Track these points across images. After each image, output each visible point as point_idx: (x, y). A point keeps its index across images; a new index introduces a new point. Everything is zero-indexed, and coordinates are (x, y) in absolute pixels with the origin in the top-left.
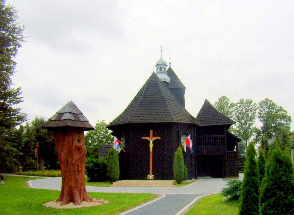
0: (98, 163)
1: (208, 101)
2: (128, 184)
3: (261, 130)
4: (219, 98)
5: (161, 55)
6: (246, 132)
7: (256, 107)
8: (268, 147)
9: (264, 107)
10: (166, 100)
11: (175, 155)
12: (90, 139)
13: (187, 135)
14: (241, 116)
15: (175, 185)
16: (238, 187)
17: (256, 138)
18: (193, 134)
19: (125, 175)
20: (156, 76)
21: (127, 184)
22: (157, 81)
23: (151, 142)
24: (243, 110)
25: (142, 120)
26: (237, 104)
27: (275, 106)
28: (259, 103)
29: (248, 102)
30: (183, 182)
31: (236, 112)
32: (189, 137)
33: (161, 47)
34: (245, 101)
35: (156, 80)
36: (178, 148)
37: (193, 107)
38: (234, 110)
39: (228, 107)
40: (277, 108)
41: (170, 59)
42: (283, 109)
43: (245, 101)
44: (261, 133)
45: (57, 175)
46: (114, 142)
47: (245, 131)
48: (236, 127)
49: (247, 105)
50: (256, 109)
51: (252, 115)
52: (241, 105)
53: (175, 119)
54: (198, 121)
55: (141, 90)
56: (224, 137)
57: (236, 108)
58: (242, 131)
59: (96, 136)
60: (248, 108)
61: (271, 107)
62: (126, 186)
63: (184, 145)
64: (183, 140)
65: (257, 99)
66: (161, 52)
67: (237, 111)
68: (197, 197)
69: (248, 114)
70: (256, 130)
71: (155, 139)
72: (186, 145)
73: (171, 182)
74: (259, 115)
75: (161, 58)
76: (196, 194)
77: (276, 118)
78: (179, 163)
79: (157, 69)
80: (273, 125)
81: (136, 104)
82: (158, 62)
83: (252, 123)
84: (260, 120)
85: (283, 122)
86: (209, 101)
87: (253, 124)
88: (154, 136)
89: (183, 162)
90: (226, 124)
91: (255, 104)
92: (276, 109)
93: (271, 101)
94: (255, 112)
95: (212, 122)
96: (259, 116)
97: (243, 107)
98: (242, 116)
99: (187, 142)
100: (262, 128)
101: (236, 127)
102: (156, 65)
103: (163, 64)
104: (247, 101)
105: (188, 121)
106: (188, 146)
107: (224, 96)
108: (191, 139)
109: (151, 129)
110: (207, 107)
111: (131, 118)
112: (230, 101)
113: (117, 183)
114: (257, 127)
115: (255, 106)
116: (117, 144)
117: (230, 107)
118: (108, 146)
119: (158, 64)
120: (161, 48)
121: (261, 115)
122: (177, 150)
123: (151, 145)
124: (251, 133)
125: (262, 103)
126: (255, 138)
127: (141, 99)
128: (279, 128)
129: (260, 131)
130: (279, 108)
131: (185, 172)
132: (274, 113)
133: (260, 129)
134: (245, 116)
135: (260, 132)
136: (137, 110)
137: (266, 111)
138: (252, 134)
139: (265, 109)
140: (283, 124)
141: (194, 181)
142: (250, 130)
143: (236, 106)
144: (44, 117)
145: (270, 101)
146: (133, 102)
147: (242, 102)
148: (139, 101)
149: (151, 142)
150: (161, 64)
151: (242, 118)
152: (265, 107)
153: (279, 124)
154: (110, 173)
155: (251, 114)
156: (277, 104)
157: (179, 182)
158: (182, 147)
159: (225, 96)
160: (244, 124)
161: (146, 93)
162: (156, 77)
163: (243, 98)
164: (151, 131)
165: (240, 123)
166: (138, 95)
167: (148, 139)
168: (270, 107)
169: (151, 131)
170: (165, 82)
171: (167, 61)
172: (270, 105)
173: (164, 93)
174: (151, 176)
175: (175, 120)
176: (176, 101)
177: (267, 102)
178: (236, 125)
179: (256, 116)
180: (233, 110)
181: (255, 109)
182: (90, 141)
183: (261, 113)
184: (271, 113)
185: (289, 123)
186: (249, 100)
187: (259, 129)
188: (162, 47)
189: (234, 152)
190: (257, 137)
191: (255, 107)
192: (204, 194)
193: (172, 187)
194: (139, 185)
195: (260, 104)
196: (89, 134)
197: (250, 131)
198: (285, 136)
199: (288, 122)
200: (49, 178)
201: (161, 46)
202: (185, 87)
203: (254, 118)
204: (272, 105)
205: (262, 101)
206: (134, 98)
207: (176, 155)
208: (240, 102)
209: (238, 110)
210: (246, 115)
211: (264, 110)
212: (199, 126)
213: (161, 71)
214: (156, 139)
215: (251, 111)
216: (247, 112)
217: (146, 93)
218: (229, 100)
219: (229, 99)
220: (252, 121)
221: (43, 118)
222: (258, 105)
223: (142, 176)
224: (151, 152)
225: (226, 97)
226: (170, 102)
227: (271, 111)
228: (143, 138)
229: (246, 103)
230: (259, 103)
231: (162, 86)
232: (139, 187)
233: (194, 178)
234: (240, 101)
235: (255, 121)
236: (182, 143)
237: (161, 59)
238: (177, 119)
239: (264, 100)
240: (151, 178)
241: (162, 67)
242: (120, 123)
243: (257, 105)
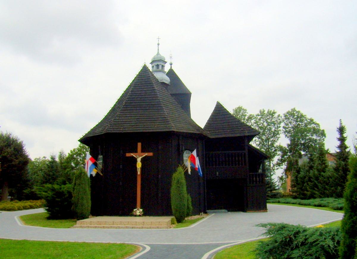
0: (61, 191)
1: (221, 104)
2: (100, 224)
3: (287, 149)
4: (233, 110)
5: (157, 49)
6: (269, 150)
7: (281, 119)
8: (300, 168)
9: (290, 119)
10: (161, 101)
11: (173, 179)
12: (73, 161)
13: (192, 151)
14: (262, 131)
15: (173, 225)
16: (291, 241)
17: (282, 158)
18: (200, 149)
19: (102, 208)
20: (148, 70)
21: (98, 224)
22: (150, 77)
23: (139, 159)
24: (264, 123)
25: (127, 129)
26: (256, 116)
27: (304, 118)
28: (284, 114)
29: (270, 114)
30: (186, 219)
31: (255, 126)
32: (195, 153)
33: (158, 39)
34: (266, 112)
35: (148, 75)
36: (178, 169)
37: (200, 115)
38: (252, 124)
39: (246, 120)
40: (306, 120)
41: (171, 58)
42: (314, 121)
43: (266, 112)
44: (287, 152)
45: (17, 209)
46: (86, 161)
47: (268, 150)
48: (256, 145)
49: (268, 117)
50: (280, 122)
51: (276, 129)
52: (261, 118)
53: (173, 127)
54: (207, 131)
55: (127, 89)
57: (255, 121)
58: (264, 149)
59: (81, 157)
60: (271, 121)
61: (299, 120)
62: (96, 227)
63: (188, 164)
64: (186, 156)
65: (281, 110)
66: (157, 46)
67: (256, 124)
68: (206, 252)
69: (270, 128)
70: (281, 149)
71: (144, 156)
72: (191, 164)
73: (166, 220)
74: (284, 129)
76: (204, 245)
77: (305, 133)
78: (180, 191)
79: (153, 67)
80: (303, 142)
81: (118, 108)
82: (154, 58)
83: (276, 139)
84: (286, 136)
85: (314, 137)
86: (222, 105)
87: (277, 141)
88: (143, 151)
89: (185, 189)
90: (247, 134)
91: (279, 116)
92: (306, 121)
93: (298, 112)
94: (279, 125)
96: (285, 130)
97: (264, 120)
98: (263, 131)
99: (192, 160)
100: (288, 145)
101: (256, 145)
102: (151, 62)
103: (161, 60)
104: (269, 113)
105: (194, 130)
106: (193, 166)
107: (240, 107)
108: (198, 155)
109: (139, 142)
110: (219, 110)
111: (110, 126)
112: (247, 113)
113: (84, 222)
114: (282, 145)
115: (279, 118)
116: (90, 163)
117: (247, 120)
119: (154, 60)
120: (158, 40)
121: (287, 130)
122: (175, 171)
123: (139, 165)
124: (275, 152)
125: (288, 115)
126: (281, 158)
127: (126, 100)
128: (309, 145)
129: (286, 149)
130: (309, 121)
131: (188, 204)
132: (303, 127)
133: (286, 146)
134: (267, 131)
135: (287, 151)
136: (120, 116)
137: (293, 125)
138: (276, 153)
139: (292, 122)
140: (316, 140)
141: (203, 218)
142: (273, 148)
143: (255, 119)
144: (11, 133)
145: (297, 112)
146: (116, 106)
147: (262, 113)
148: (123, 104)
149: (139, 159)
150: (158, 60)
151: (264, 134)
152: (292, 120)
153: (311, 140)
154: (76, 207)
155: (274, 128)
156: (305, 115)
157: (180, 220)
158: (185, 168)
159: (242, 107)
160: (266, 141)
161: (133, 93)
162: (147, 71)
163: (263, 109)
164: (139, 145)
165: (260, 140)
166: (122, 97)
167: (134, 156)
168: (297, 119)
169: (139, 145)
170: (163, 83)
171: (165, 58)
172: (298, 117)
173: (159, 95)
174: (138, 211)
175: (174, 129)
176: (174, 100)
177: (293, 113)
178: (256, 142)
179: (280, 130)
180: (252, 124)
181: (279, 122)
182: (73, 164)
183: (287, 127)
184: (300, 127)
185: (323, 139)
186: (271, 111)
187: (285, 148)
189: (259, 175)
190: (282, 157)
191: (279, 119)
192: (218, 244)
193: (167, 228)
194: (118, 225)
195: (285, 116)
196: (71, 155)
197: (273, 150)
198: (322, 153)
199: (321, 137)
202: (191, 92)
203: (278, 134)
204: (300, 117)
205: (287, 112)
206: (117, 100)
207: (175, 178)
208: (260, 113)
209: (258, 123)
210: (268, 129)
211: (290, 123)
212: (209, 138)
213: (158, 70)
215: (275, 124)
216: (269, 127)
217: (133, 93)
218: (247, 112)
219: (246, 110)
220: (276, 137)
221: (10, 134)
222: (283, 117)
223: (126, 211)
224: (139, 175)
225: (243, 108)
226: (168, 105)
227: (299, 125)
228: (128, 155)
229: (268, 114)
230: (284, 114)
231: (156, 83)
233: (202, 213)
234: (260, 112)
235: (280, 137)
236: (184, 161)
237: (158, 54)
238: (175, 127)
239: (290, 111)
240: (138, 213)
241: (159, 64)
242: (96, 134)
243: (281, 118)
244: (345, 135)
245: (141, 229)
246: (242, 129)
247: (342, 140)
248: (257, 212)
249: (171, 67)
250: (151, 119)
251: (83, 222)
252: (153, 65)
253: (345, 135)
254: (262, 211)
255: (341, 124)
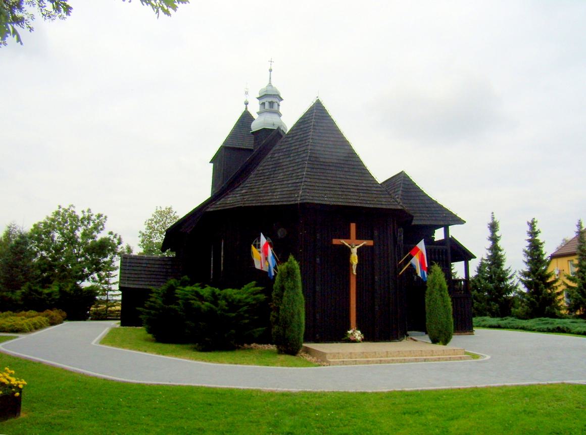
5: (269, 78)
23: (354, 251)
56: (446, 250)
66: (269, 72)
71: (361, 245)
75: (270, 83)
79: (263, 104)
88: (359, 237)
95: (426, 218)
102: (259, 96)
118: (138, 259)
123: (354, 259)
149: (354, 251)
150: (274, 95)
164: (353, 226)
167: (347, 244)
169: (353, 226)
171: (280, 91)
188: (271, 62)
200: (17, 337)
201: (272, 63)
213: (272, 109)
214: (364, 246)
228: (335, 241)
232: (377, 363)
244: (498, 234)
245: (438, 362)
246: (444, 215)
247: (494, 239)
248: (458, 335)
249: (246, 108)
250: (358, 188)
251: (337, 355)
252: (264, 101)
253: (498, 234)
254: (468, 333)
255: (493, 218)
